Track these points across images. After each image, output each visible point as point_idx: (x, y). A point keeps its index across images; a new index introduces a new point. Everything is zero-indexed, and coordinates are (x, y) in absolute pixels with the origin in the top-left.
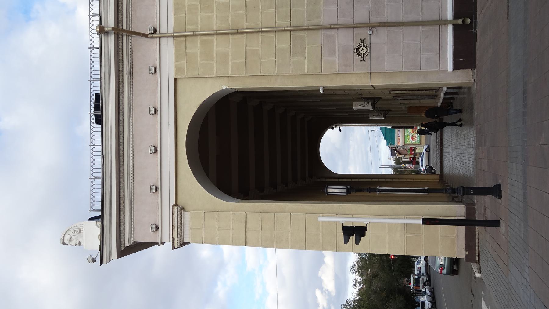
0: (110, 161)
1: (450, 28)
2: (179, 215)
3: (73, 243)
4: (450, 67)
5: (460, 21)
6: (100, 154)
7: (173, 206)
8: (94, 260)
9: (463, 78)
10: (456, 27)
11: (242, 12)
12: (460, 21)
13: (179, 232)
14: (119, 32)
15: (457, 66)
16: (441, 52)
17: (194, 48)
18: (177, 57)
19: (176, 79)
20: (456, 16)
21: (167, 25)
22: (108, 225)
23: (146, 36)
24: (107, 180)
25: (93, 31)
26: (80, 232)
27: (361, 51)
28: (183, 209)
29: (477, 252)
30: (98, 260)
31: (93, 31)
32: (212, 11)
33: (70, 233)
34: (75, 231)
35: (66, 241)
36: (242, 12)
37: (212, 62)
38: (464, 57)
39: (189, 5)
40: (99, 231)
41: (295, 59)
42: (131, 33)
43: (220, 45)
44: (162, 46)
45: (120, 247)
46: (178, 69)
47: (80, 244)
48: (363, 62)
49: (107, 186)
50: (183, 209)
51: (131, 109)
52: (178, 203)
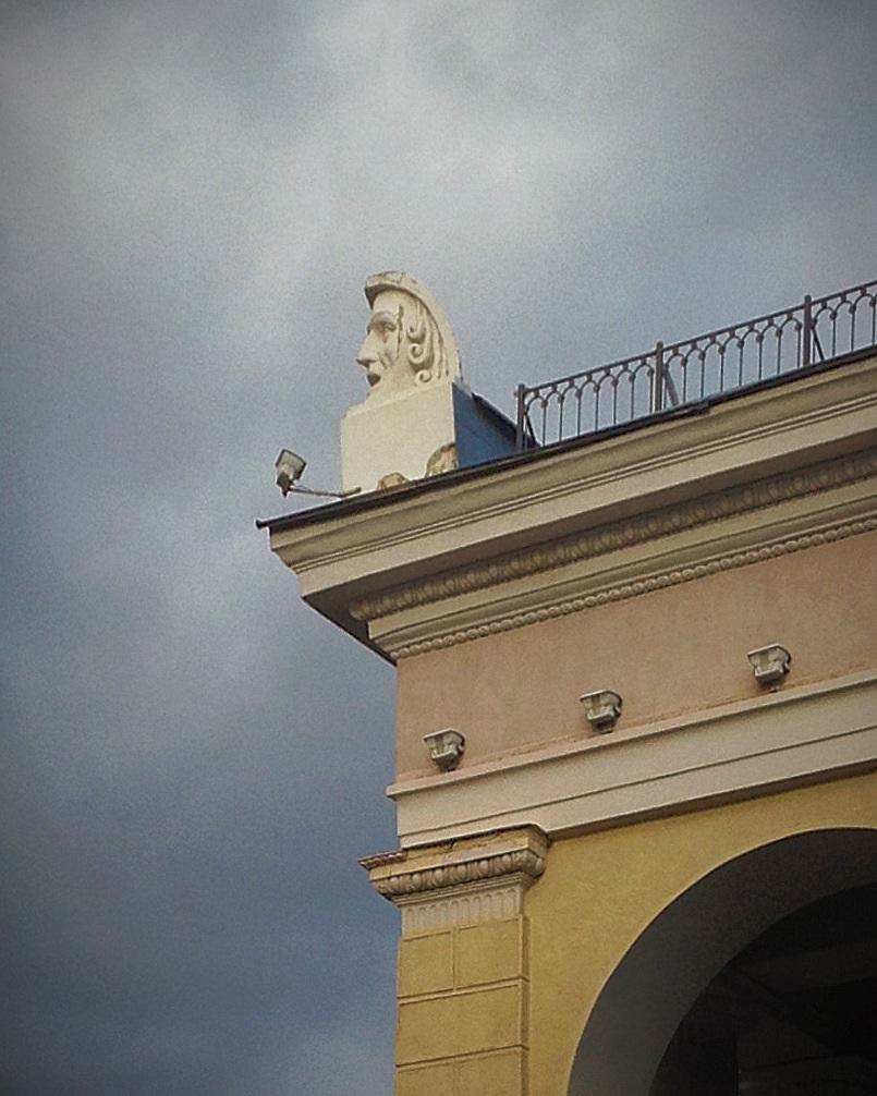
0: (690, 451)
2: (498, 865)
3: (372, 347)
6: (713, 390)
8: (285, 484)
13: (476, 870)
22: (422, 517)
24: (608, 460)
26: (416, 368)
28: (530, 875)
30: (297, 504)
33: (413, 319)
34: (420, 340)
35: (387, 306)
40: (416, 473)
45: (359, 601)
47: (374, 379)
49: (583, 468)
51: (552, 611)
52: (561, 850)
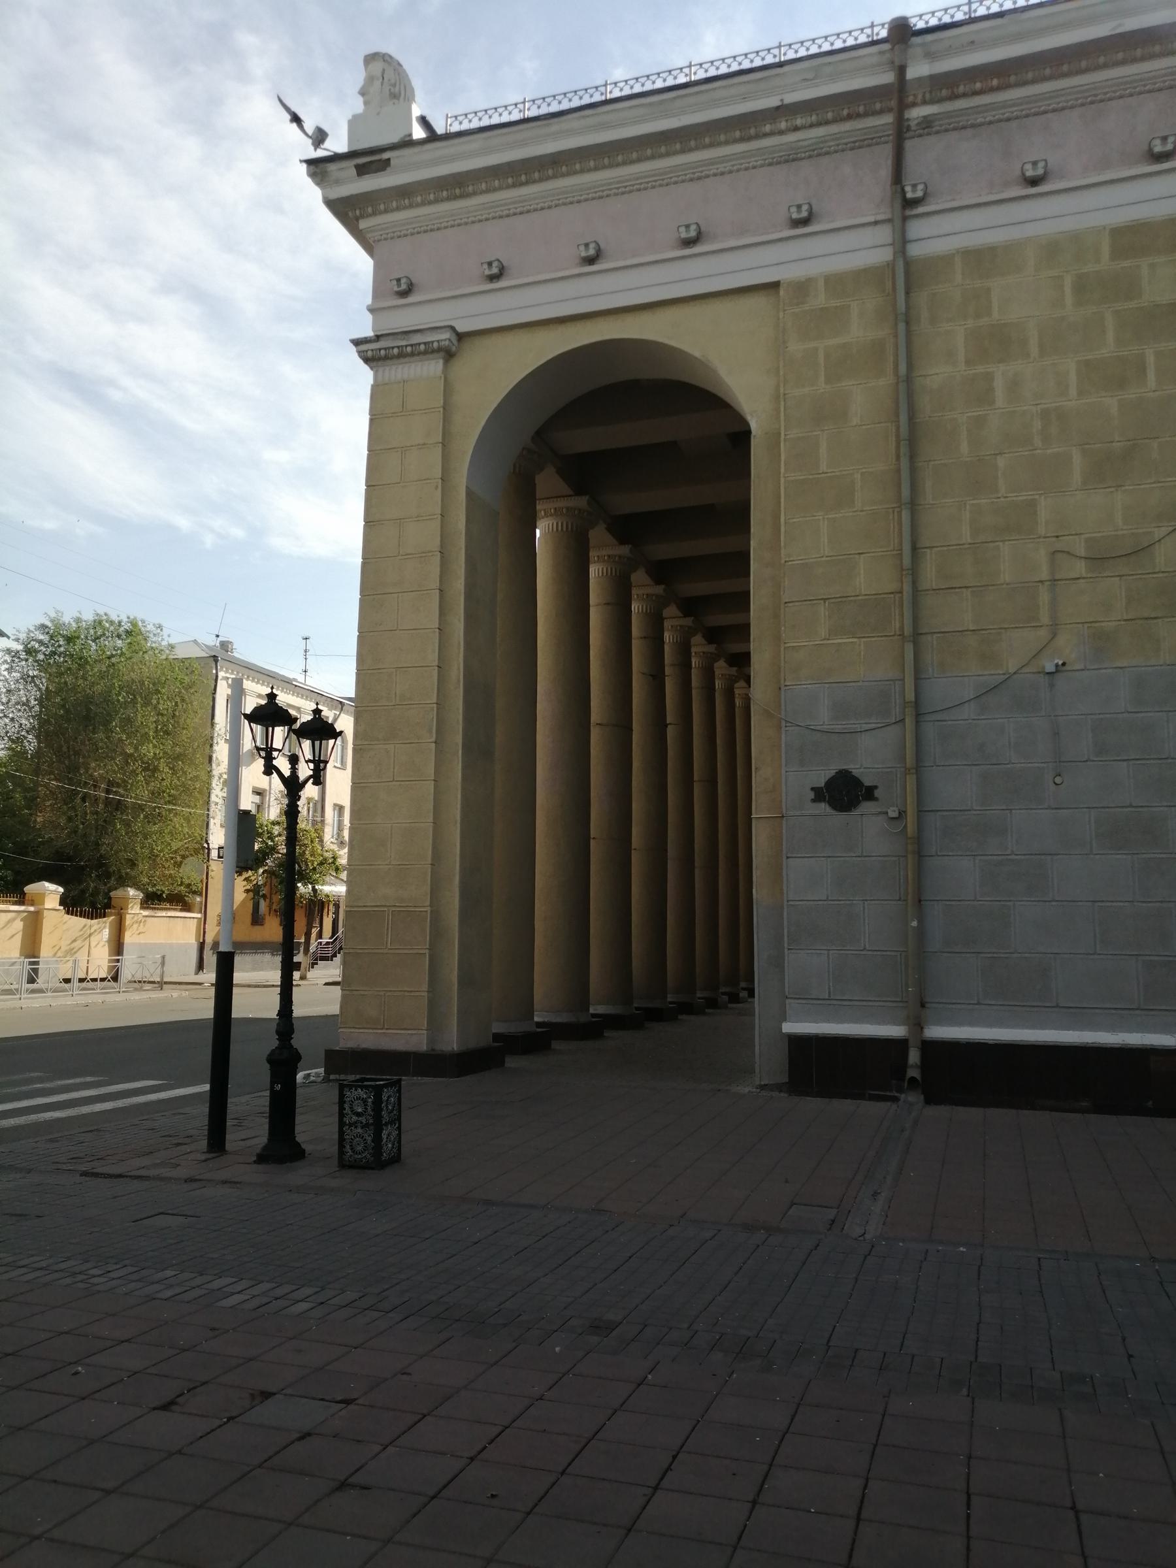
1: (894, 1031)
4: (789, 1028)
5: (914, 1057)
7: (452, 328)
9: (769, 1063)
10: (899, 1046)
11: (964, 448)
12: (914, 1057)
14: (899, 94)
15: (798, 1043)
16: (831, 1007)
17: (861, 326)
18: (837, 283)
19: (775, 285)
20: (932, 1048)
21: (934, 236)
23: (898, 177)
25: (505, 114)
27: (844, 792)
28: (449, 355)
29: (1156, 958)
31: (505, 114)
32: (968, 362)
36: (964, 448)
37: (822, 379)
38: (822, 1067)
39: (989, 290)
41: (822, 610)
42: (901, 133)
43: (866, 398)
44: (869, 231)
46: (802, 288)
48: (812, 795)
50: (449, 355)
